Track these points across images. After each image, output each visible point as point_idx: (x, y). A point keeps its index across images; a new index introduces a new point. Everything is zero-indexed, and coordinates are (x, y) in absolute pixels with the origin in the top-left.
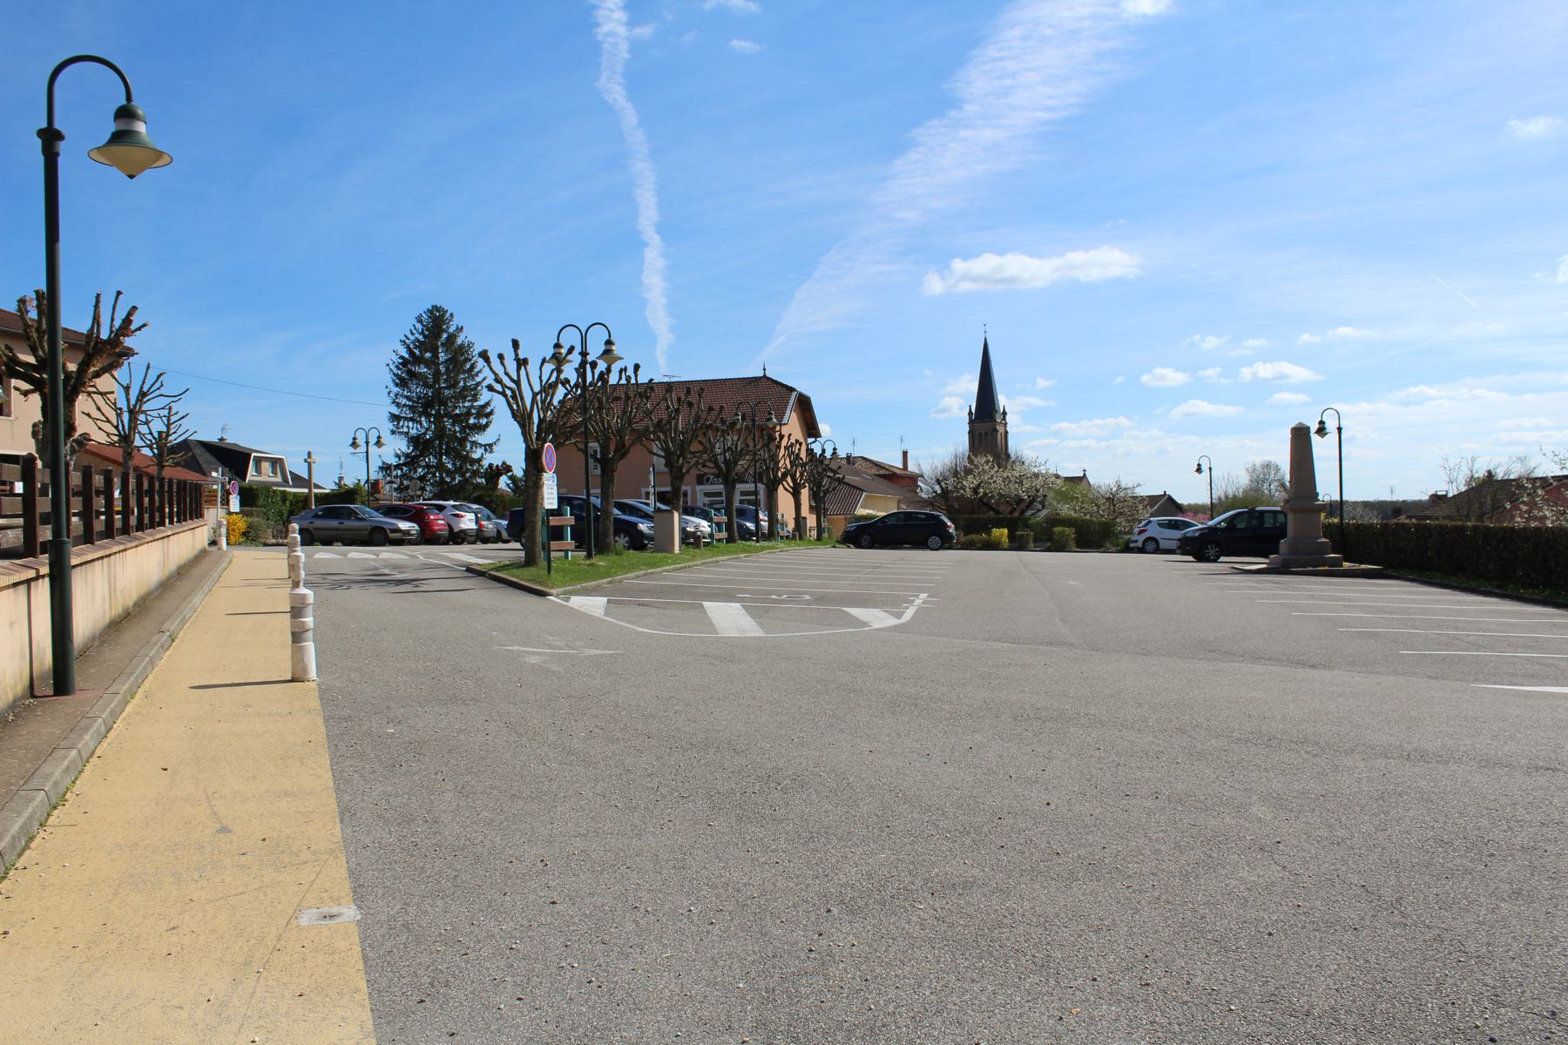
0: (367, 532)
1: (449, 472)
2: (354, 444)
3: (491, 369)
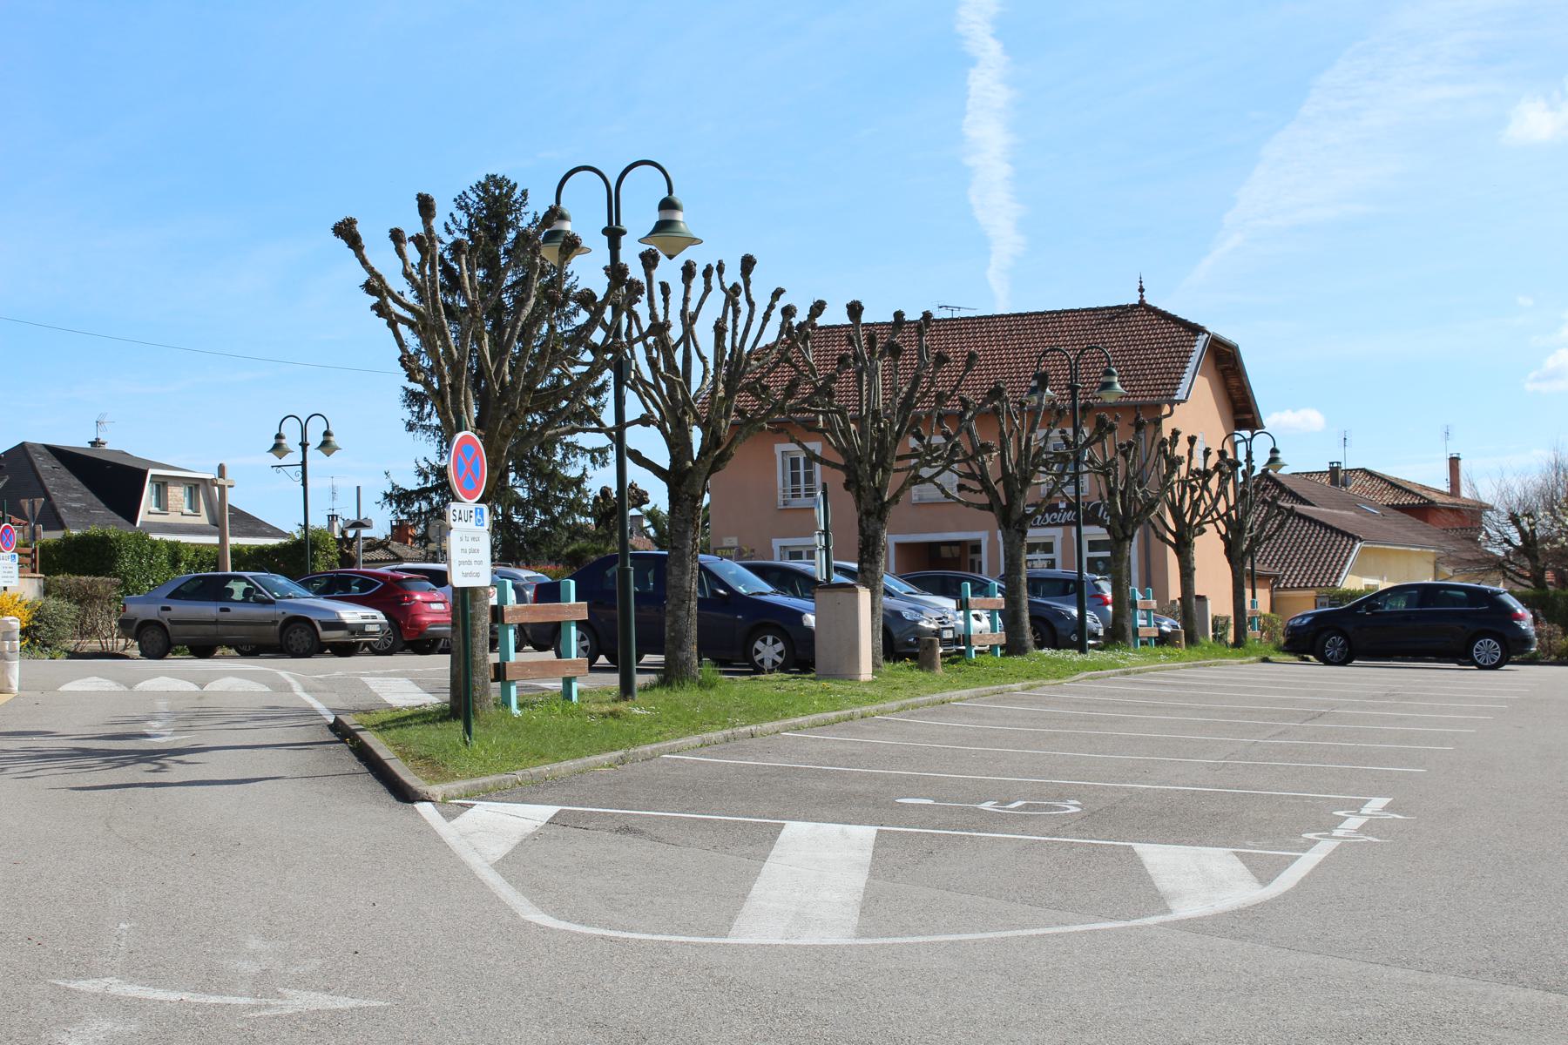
0: (277, 627)
1: (520, 504)
2: (278, 448)
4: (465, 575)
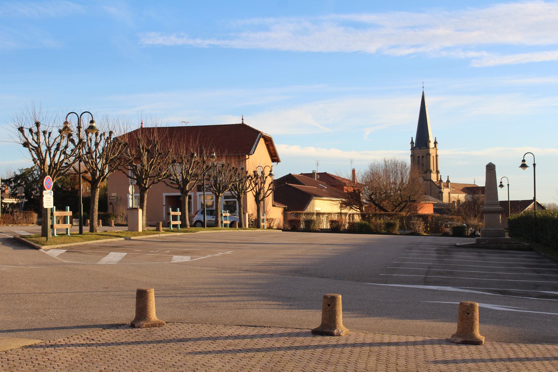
3: (24, 136)
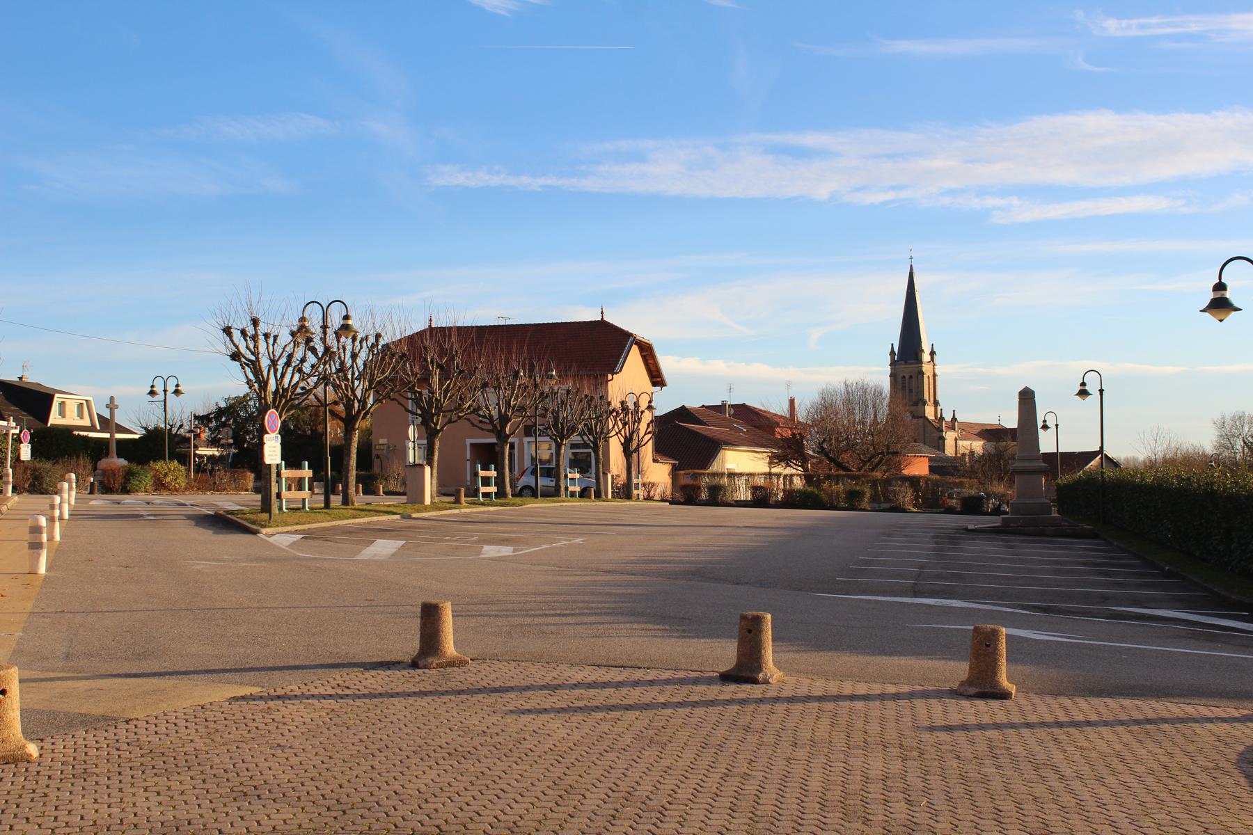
2: (152, 393)
4: (271, 459)
